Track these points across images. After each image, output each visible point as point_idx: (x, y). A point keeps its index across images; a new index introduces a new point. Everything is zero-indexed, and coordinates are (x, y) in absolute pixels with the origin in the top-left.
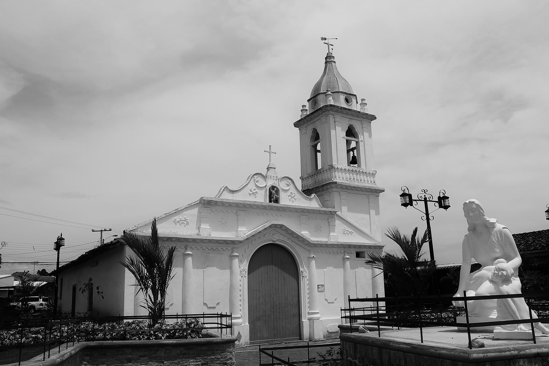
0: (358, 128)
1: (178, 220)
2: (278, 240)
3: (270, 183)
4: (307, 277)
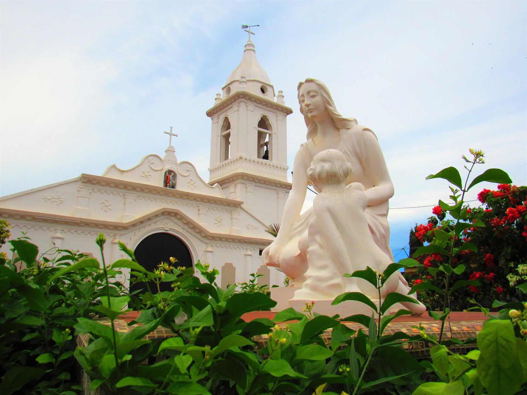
0: (272, 119)
2: (171, 229)
3: (167, 167)
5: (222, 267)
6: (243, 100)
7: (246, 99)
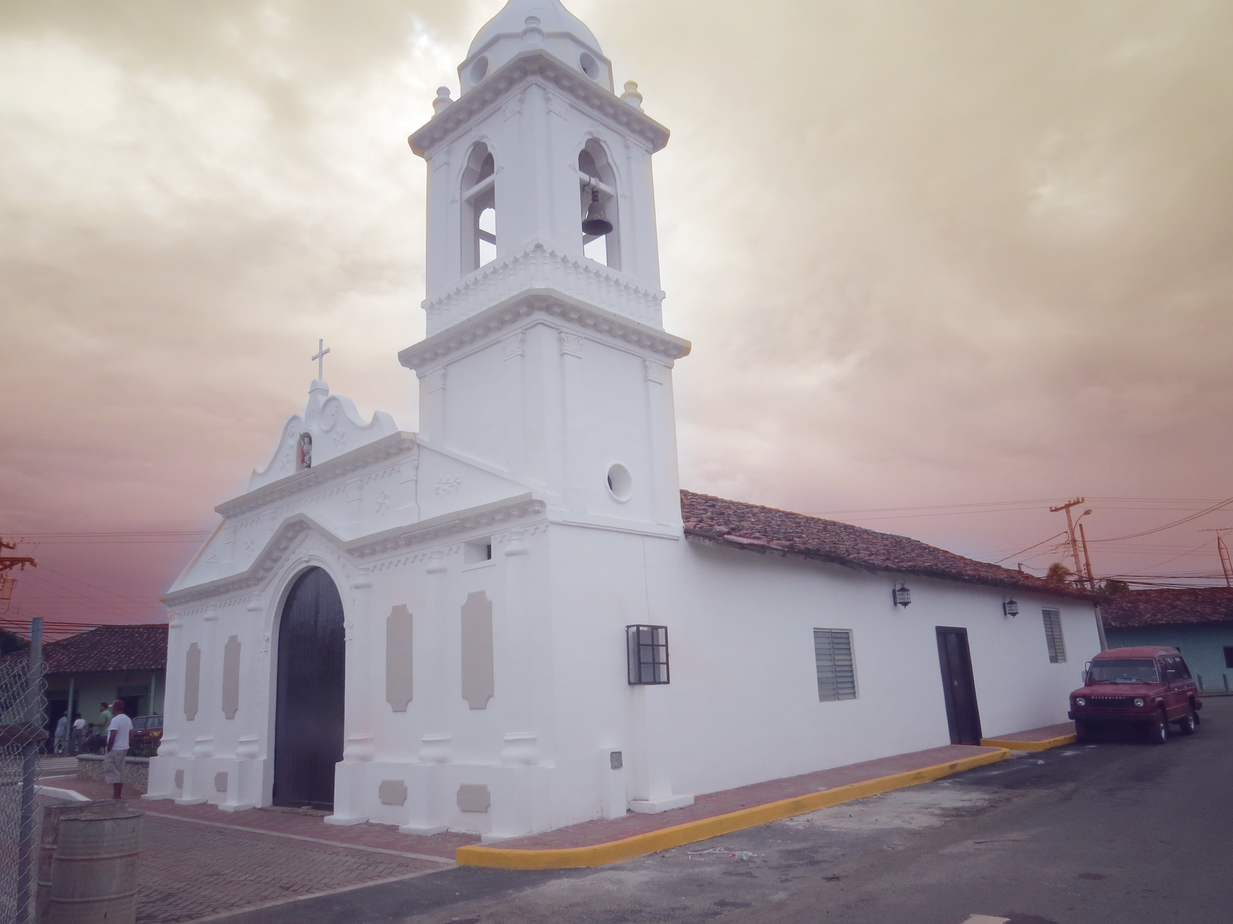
0: (615, 149)
5: (483, 593)
6: (538, 79)
7: (547, 78)
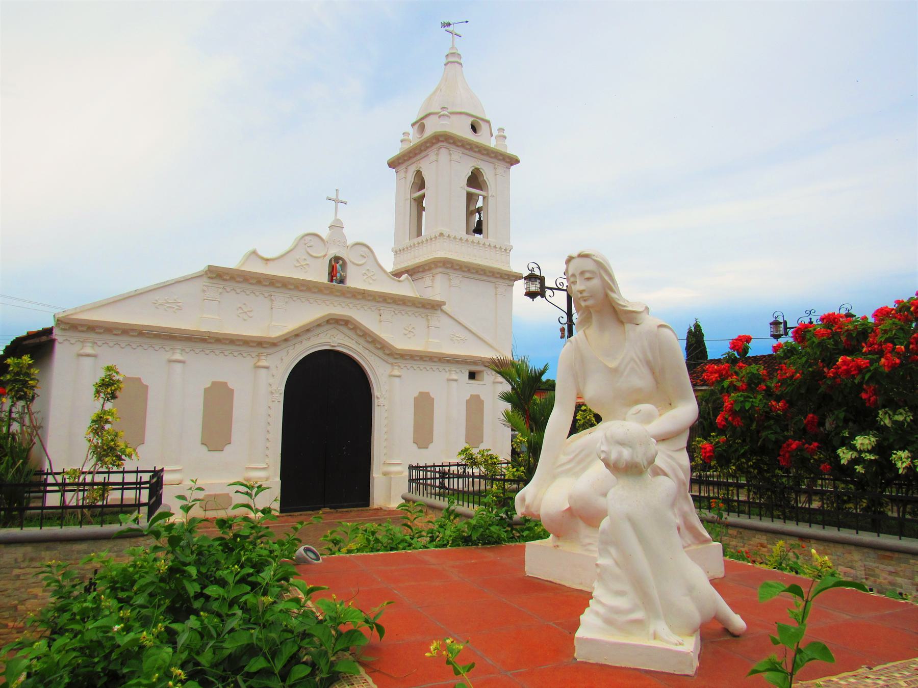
0: (489, 173)
1: (160, 302)
2: (340, 345)
3: (333, 252)
4: (386, 408)
